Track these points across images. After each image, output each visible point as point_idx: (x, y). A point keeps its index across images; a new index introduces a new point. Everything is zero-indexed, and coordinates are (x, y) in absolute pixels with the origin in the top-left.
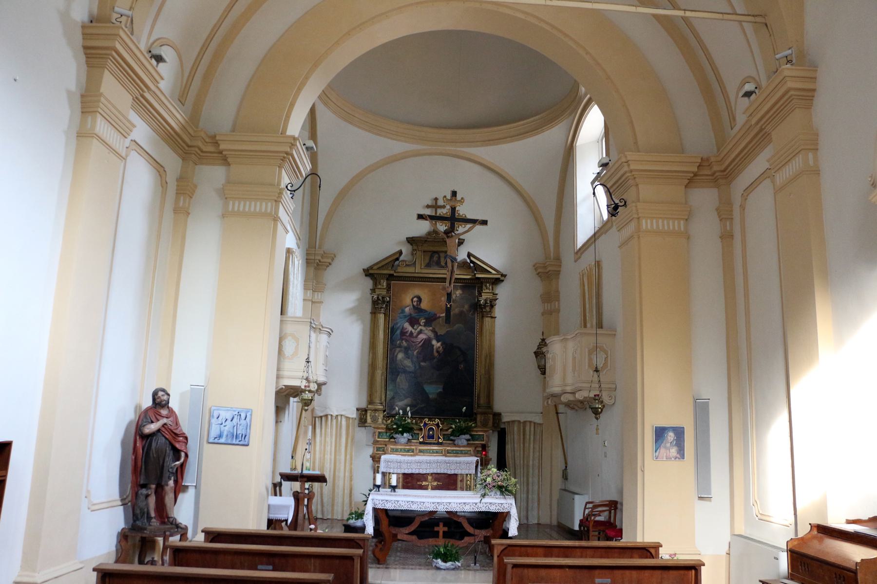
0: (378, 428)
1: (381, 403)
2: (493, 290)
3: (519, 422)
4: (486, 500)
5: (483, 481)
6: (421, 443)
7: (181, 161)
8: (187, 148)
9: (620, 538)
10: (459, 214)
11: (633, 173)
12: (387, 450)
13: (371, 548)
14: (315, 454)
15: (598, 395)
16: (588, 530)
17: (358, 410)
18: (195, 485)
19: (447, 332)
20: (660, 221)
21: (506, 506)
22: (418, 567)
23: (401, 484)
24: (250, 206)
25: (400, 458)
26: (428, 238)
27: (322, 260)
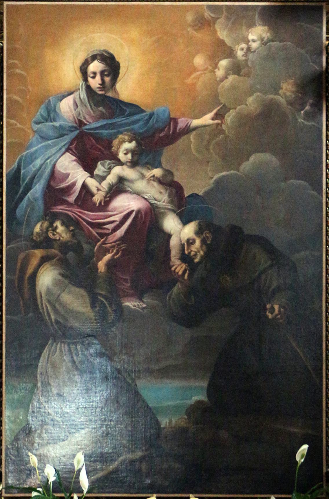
19: (218, 182)
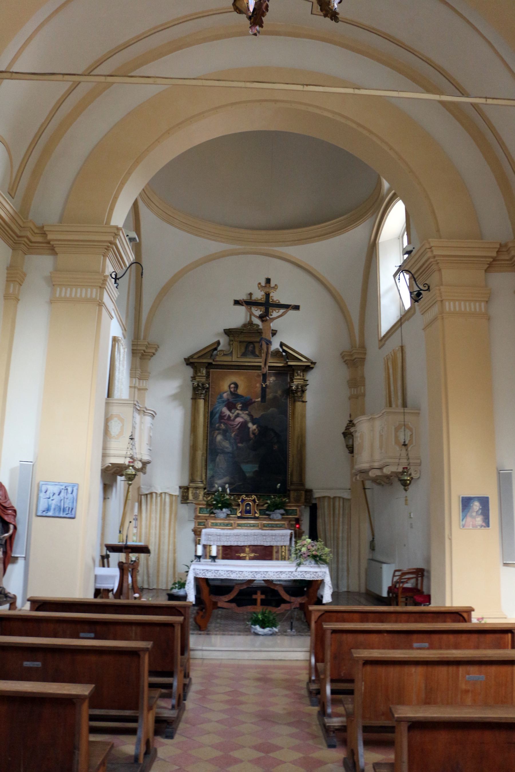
1: (202, 482)
2: (303, 377)
3: (329, 497)
4: (302, 569)
5: (298, 551)
6: (239, 518)
7: (11, 251)
8: (16, 238)
9: (428, 604)
10: (273, 300)
11: (437, 258)
12: (208, 524)
13: (193, 616)
14: (141, 529)
15: (406, 468)
16: (397, 596)
17: (180, 488)
18: (24, 556)
20: (462, 303)
21: (320, 574)
22: (237, 633)
23: (220, 556)
24: (76, 292)
25: (219, 531)
26: (244, 330)
27: (147, 351)
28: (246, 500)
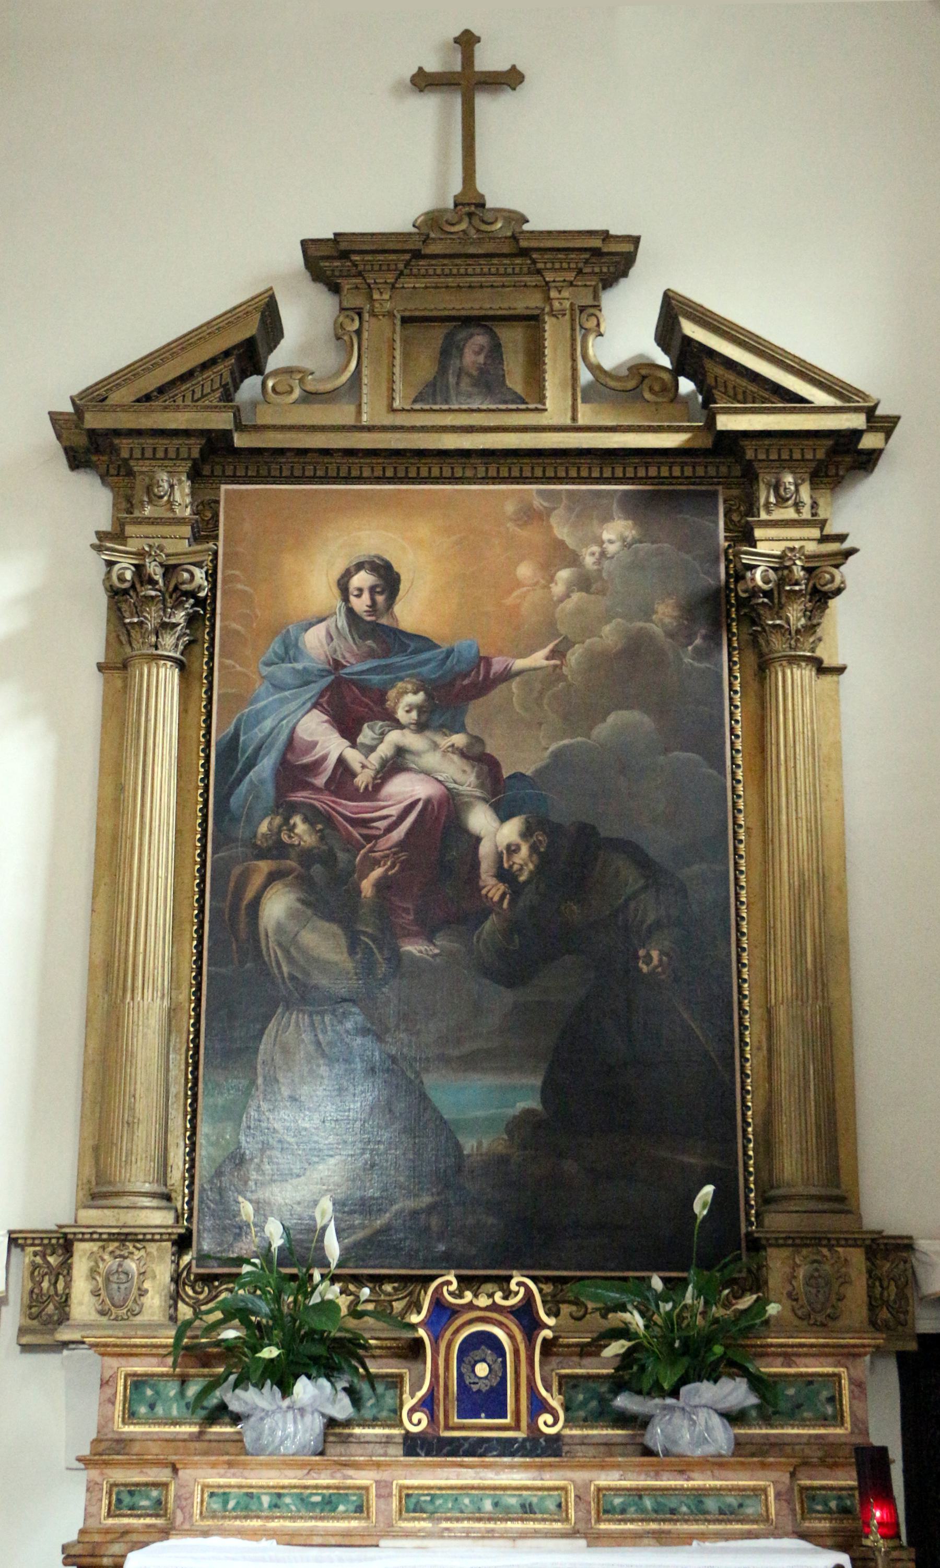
0: (129, 1352)
1: (168, 1198)
12: (183, 1501)
28: (471, 1306)
